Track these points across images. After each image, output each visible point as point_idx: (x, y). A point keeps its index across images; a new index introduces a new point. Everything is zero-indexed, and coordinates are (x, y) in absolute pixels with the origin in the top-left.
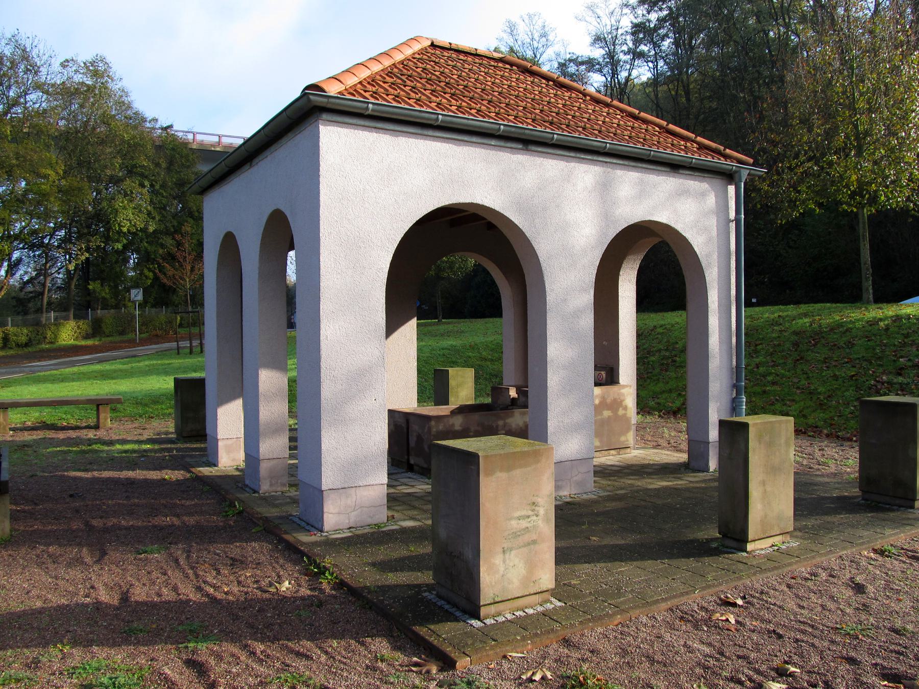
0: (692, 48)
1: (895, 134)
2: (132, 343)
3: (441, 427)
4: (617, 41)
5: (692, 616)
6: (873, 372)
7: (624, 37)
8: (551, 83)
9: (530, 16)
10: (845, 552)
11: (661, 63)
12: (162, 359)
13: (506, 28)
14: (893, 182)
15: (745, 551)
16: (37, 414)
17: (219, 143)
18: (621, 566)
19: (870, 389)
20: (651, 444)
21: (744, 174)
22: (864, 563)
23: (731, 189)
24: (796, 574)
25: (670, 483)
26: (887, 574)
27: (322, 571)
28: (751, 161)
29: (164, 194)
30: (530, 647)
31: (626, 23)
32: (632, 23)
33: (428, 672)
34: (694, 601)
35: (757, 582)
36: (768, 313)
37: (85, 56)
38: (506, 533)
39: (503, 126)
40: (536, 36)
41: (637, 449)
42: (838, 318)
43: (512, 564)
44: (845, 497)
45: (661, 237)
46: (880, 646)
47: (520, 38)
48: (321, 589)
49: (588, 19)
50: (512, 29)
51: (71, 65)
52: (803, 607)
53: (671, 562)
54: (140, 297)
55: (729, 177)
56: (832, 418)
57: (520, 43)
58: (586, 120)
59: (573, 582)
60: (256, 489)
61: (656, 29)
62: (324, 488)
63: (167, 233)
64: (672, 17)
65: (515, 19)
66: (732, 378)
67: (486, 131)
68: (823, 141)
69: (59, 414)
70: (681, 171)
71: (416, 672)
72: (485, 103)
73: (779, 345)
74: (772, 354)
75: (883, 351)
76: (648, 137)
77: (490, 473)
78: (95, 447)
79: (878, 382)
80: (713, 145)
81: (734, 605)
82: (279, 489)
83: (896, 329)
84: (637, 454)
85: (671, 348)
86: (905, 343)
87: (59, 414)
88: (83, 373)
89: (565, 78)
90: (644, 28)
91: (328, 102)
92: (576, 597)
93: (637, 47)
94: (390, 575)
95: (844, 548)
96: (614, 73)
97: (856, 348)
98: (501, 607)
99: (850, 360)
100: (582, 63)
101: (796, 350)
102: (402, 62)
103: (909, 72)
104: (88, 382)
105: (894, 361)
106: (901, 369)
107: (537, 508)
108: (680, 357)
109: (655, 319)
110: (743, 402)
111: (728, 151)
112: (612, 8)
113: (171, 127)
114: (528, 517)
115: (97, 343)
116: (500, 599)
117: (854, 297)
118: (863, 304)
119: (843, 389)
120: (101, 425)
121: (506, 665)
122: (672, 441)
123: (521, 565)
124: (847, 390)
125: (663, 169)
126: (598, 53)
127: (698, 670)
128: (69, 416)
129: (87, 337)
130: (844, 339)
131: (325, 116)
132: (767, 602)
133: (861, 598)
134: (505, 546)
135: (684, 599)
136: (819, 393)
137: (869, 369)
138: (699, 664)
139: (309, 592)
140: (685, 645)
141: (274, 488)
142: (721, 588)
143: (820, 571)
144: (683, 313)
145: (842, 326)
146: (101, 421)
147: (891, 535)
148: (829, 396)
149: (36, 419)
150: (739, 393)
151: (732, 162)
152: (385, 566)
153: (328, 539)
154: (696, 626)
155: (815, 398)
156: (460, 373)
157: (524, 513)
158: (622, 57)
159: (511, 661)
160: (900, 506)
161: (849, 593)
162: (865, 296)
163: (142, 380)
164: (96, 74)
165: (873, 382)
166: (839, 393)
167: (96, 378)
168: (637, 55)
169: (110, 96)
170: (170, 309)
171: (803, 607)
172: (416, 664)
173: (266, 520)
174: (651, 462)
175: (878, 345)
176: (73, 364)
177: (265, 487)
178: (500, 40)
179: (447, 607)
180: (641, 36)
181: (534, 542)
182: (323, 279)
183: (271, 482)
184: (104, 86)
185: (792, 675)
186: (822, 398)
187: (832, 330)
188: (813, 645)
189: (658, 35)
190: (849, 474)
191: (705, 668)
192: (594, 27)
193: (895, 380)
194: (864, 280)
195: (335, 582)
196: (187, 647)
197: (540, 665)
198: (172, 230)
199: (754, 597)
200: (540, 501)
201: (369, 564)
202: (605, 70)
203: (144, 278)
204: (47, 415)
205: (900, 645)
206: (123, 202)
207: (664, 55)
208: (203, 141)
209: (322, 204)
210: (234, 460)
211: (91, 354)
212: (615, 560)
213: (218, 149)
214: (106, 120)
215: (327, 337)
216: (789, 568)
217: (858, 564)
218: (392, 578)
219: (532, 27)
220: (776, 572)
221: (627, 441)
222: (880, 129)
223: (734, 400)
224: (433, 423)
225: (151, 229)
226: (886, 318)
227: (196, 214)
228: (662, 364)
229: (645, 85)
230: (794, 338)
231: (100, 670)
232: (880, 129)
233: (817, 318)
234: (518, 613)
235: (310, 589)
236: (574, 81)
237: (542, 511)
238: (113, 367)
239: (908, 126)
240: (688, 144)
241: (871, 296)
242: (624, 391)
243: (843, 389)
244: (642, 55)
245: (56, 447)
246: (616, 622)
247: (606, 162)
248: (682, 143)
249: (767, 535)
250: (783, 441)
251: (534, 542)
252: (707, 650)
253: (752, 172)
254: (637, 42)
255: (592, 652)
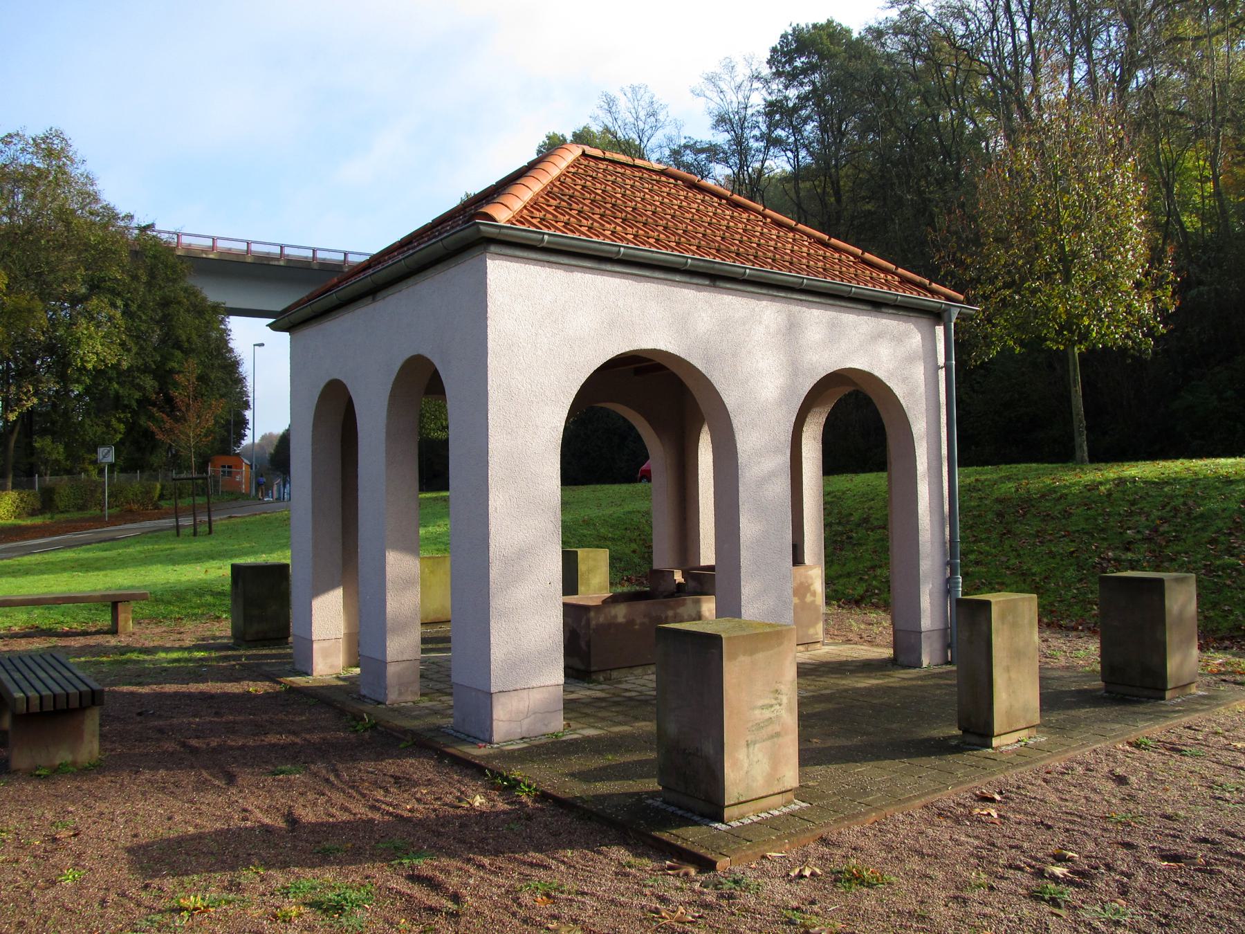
0: (843, 134)
1: (1110, 258)
2: (98, 521)
3: (601, 620)
4: (746, 124)
5: (951, 812)
6: (1096, 547)
7: (754, 119)
8: (724, 202)
9: (633, 89)
10: (1103, 745)
11: (803, 153)
12: (156, 542)
13: (602, 104)
14: (1107, 315)
15: (990, 746)
16: (25, 617)
17: (213, 247)
18: (857, 767)
19: (1094, 567)
20: (840, 640)
21: (955, 314)
22: (1120, 756)
23: (940, 330)
24: (1050, 768)
25: (880, 681)
26: (1148, 766)
27: (514, 785)
28: (961, 297)
29: (144, 318)
30: (787, 846)
31: (758, 100)
32: (765, 100)
33: (686, 874)
34: (948, 797)
35: (1012, 776)
36: (988, 474)
37: (36, 130)
38: (750, 724)
39: (690, 257)
40: (642, 114)
41: (828, 644)
42: (1049, 482)
43: (755, 759)
44: (1086, 690)
45: (855, 384)
46: (1155, 831)
47: (620, 117)
48: (521, 803)
49: (708, 93)
50: (610, 105)
51: (15, 141)
52: (1066, 800)
53: (911, 761)
54: (111, 458)
55: (937, 316)
56: (1051, 604)
57: (620, 122)
58: (688, 221)
59: (811, 784)
60: (380, 700)
61: (796, 109)
62: (493, 690)
63: (145, 370)
64: (816, 95)
65: (615, 92)
66: (945, 554)
67: (661, 264)
68: (1024, 264)
69: (55, 616)
70: (883, 310)
71: (673, 875)
72: (587, 202)
73: (980, 516)
74: (971, 527)
75: (1106, 522)
76: (844, 269)
77: (733, 657)
78: (134, 656)
79: (1103, 559)
80: (918, 278)
81: (993, 800)
82: (409, 698)
83: (1120, 495)
84: (827, 651)
85: (843, 521)
86: (1132, 512)
87: (55, 616)
88: (52, 563)
89: (679, 169)
90: (782, 107)
91: (499, 233)
92: (821, 798)
93: (770, 132)
94: (598, 785)
95: (1098, 742)
96: (743, 165)
97: (1074, 518)
98: (744, 807)
99: (1068, 534)
100: (702, 151)
101: (1001, 522)
102: (558, 179)
103: (1123, 182)
104: (65, 575)
105: (1121, 533)
106: (1129, 543)
107: (780, 696)
108: (857, 533)
109: (844, 482)
110: (958, 583)
111: (934, 285)
112: (738, 80)
113: (150, 227)
114: (772, 706)
115: (48, 522)
116: (744, 799)
117: (1063, 454)
118: (1077, 464)
119: (1062, 568)
120: (120, 629)
121: (768, 865)
122: (864, 635)
123: (765, 760)
124: (1067, 570)
125: (865, 307)
126: (722, 138)
127: (972, 860)
128: (69, 619)
129: (33, 513)
130: (1059, 507)
131: (493, 248)
132: (1026, 796)
133: (1124, 789)
134: (749, 738)
135: (938, 796)
136: (1034, 574)
137: (1091, 544)
138: (972, 855)
139: (507, 807)
140: (951, 838)
141: (403, 698)
142: (975, 784)
143: (1075, 765)
144: (885, 475)
145: (1055, 492)
146: (121, 623)
147: (1145, 727)
148: (1046, 578)
149: (25, 622)
150: (953, 572)
151: (940, 298)
152: (585, 776)
153: (502, 751)
154: (957, 821)
155: (1029, 580)
156: (591, 555)
157: (767, 701)
158: (754, 144)
159: (772, 860)
160: (1149, 698)
161: (1111, 785)
162: (1078, 454)
163: (142, 570)
164: (50, 154)
165: (1097, 560)
166: (1058, 574)
167: (72, 568)
168: (772, 142)
169: (68, 183)
170: (146, 474)
171: (1066, 800)
172: (670, 868)
173: (413, 733)
174: (850, 659)
175: (1099, 515)
176: (29, 551)
177: (392, 697)
178: (595, 119)
179: (680, 812)
180: (777, 117)
181: (778, 735)
182: (491, 440)
183: (399, 690)
184: (61, 169)
185: (1071, 859)
186: (1037, 579)
187: (1043, 496)
188: (1085, 833)
189: (800, 116)
190: (1083, 667)
191: (980, 858)
192: (715, 104)
193: (1123, 557)
194: (1076, 434)
195: (536, 795)
196: (401, 864)
197: (804, 862)
198: (154, 367)
199: (1011, 792)
200: (784, 688)
201: (567, 775)
202: (731, 161)
203: (113, 432)
204: (39, 617)
205: (1175, 829)
206: (87, 329)
207: (807, 142)
208: (190, 245)
209: (489, 351)
210: (331, 667)
211: (43, 536)
212: (848, 761)
213: (211, 256)
214: (65, 216)
215: (496, 509)
216: (1043, 763)
217: (1114, 757)
218: (602, 788)
219: (636, 102)
220: (1029, 767)
221: (817, 634)
222: (1089, 252)
223: (948, 581)
224: (592, 614)
225: (125, 365)
226: (1107, 481)
227: (186, 345)
228: (835, 542)
229: (785, 179)
230: (998, 507)
231: (315, 889)
232: (1089, 252)
233: (1024, 482)
234: (763, 815)
235: (508, 804)
236: (691, 173)
237: (785, 700)
238: (91, 555)
239: (1124, 247)
240: (889, 277)
241: (1086, 454)
242: (810, 573)
243: (1062, 568)
244: (777, 142)
245: (79, 657)
246: (871, 821)
247: (801, 300)
248: (882, 275)
249: (1013, 728)
250: (1026, 621)
251: (778, 735)
252: (976, 843)
253: (963, 310)
254: (772, 126)
255: (855, 849)
